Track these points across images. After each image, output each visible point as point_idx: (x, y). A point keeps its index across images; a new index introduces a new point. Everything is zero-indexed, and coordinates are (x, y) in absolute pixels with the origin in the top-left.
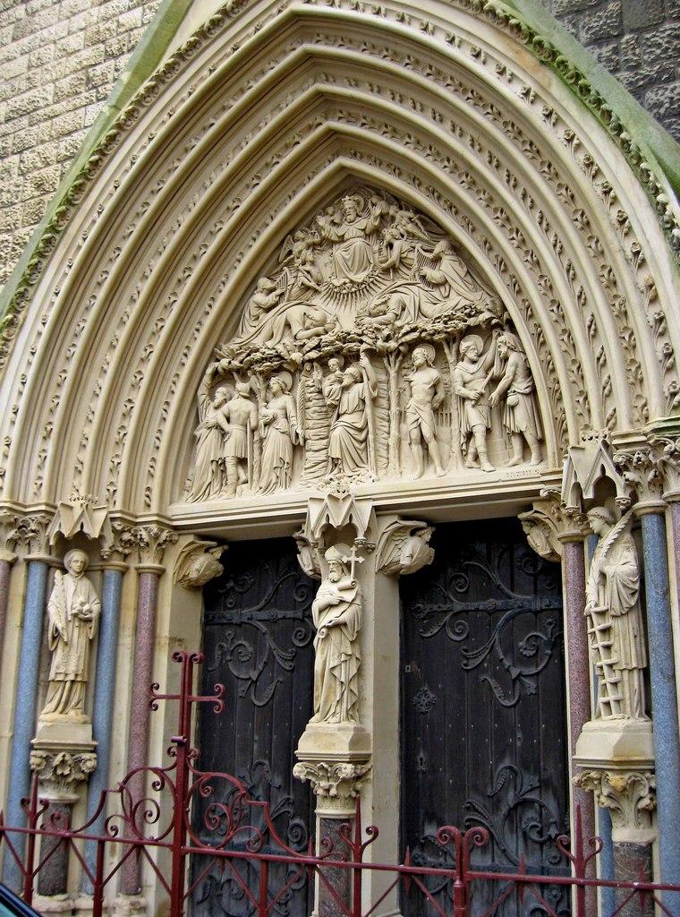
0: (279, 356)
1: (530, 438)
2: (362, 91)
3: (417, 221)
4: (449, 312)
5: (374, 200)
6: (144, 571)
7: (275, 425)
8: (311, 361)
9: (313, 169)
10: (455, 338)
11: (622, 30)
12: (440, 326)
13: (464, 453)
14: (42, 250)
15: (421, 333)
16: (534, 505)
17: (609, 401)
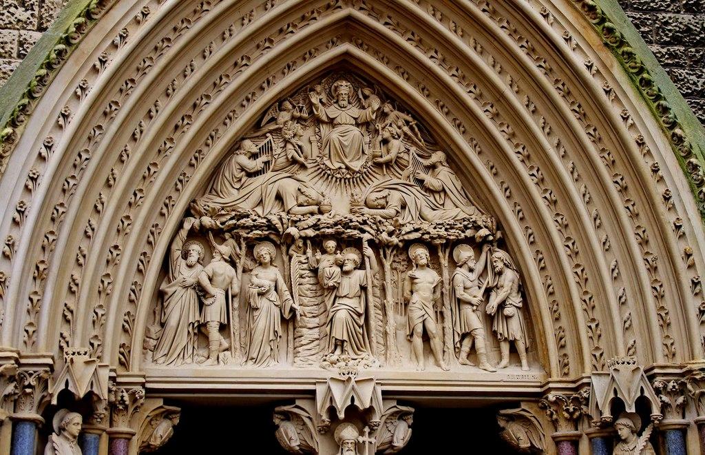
0: (270, 226)
1: (521, 347)
2: (465, 42)
3: (414, 126)
4: (452, 222)
5: (367, 92)
6: (120, 436)
7: (267, 296)
8: (305, 239)
10: (451, 245)
12: (443, 232)
13: (457, 350)
14: (54, 61)
15: (423, 234)
16: (522, 404)
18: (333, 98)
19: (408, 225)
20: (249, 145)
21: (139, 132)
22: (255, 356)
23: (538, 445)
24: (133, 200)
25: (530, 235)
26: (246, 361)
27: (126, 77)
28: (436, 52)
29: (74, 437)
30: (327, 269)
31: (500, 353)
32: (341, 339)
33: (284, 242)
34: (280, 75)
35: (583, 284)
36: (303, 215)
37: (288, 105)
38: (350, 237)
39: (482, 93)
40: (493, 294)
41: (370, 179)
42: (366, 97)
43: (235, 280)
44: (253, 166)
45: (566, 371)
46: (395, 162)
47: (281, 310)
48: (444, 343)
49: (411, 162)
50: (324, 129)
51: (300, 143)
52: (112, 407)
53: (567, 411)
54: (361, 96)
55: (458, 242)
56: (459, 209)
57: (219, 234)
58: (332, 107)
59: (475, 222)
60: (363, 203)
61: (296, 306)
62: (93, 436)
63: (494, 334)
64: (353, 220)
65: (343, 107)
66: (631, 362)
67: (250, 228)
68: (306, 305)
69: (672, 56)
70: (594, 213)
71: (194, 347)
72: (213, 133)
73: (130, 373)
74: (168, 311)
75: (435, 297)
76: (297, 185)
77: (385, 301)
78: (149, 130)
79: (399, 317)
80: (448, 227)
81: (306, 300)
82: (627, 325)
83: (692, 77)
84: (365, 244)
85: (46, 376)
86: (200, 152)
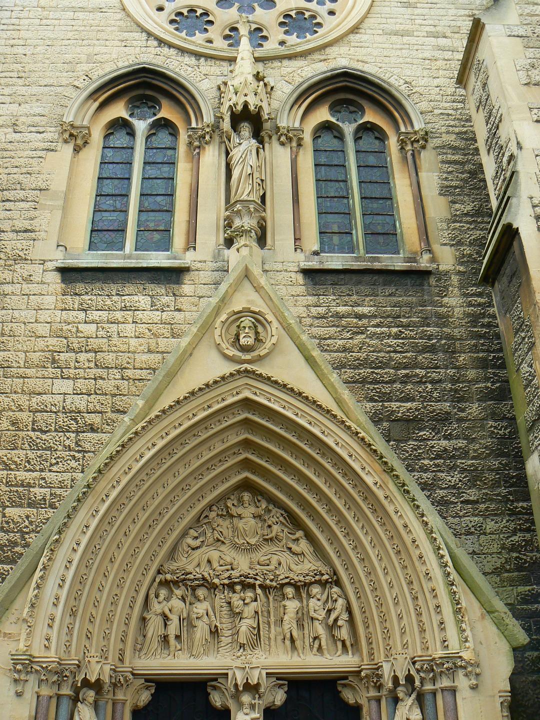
0: (204, 579)
1: (348, 644)
2: (309, 471)
4: (307, 572)
5: (259, 498)
8: (223, 585)
11: (390, 438)
12: (302, 578)
15: (290, 580)
16: (349, 677)
17: (404, 636)
20: (193, 533)
22: (194, 654)
23: (359, 701)
24: (125, 569)
27: (121, 502)
28: (295, 476)
29: (91, 704)
33: (212, 587)
35: (380, 607)
37: (214, 508)
40: (332, 612)
42: (259, 501)
43: (184, 610)
45: (372, 657)
50: (235, 520)
52: (114, 685)
53: (373, 681)
54: (256, 501)
55: (311, 583)
57: (176, 583)
59: (320, 571)
61: (218, 624)
62: (103, 702)
66: (404, 653)
67: (193, 580)
68: (224, 625)
69: (437, 466)
70: (383, 566)
73: (124, 666)
74: (147, 628)
78: (133, 530)
79: (278, 628)
82: (403, 631)
83: (448, 478)
84: (257, 587)
85: (75, 670)
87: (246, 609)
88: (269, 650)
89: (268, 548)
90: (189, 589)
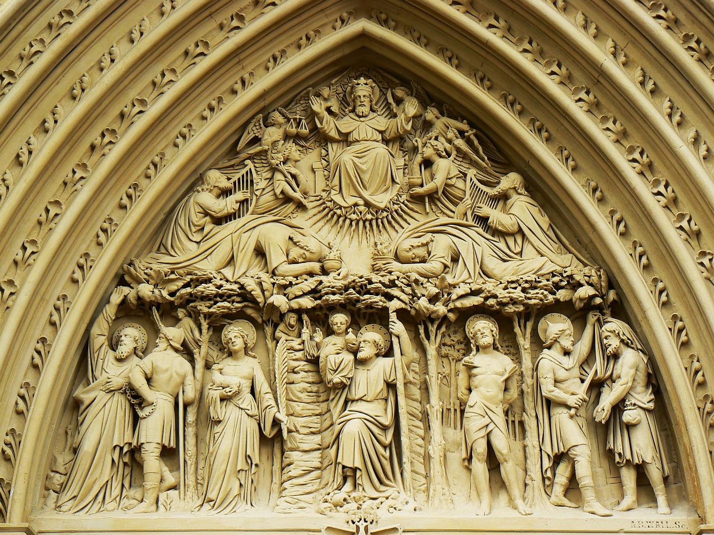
0: (245, 295)
1: (655, 474)
3: (472, 137)
4: (533, 277)
5: (400, 93)
7: (235, 400)
8: (299, 312)
9: (316, 26)
10: (535, 314)
12: (518, 294)
13: (547, 483)
15: (486, 298)
18: (349, 105)
19: (462, 285)
21: (27, 153)
25: (661, 292)
26: (202, 505)
30: (332, 358)
31: (621, 484)
32: (351, 466)
33: (267, 319)
34: (261, 70)
36: (296, 277)
38: (370, 306)
39: (570, 73)
40: (605, 390)
41: (406, 221)
42: (399, 101)
43: (189, 379)
44: (221, 207)
46: (443, 192)
47: (259, 424)
48: (526, 471)
49: (468, 192)
50: (334, 150)
51: (294, 171)
54: (391, 100)
55: (545, 310)
56: (545, 259)
57: (169, 311)
58: (347, 118)
60: (392, 255)
61: (282, 416)
63: (610, 454)
64: (374, 280)
65: (363, 117)
67: (212, 299)
68: (300, 416)
71: (123, 486)
72: (157, 159)
75: (508, 397)
76: (289, 232)
77: (428, 406)
78: (41, 150)
79: (450, 432)
80: (527, 285)
81: (298, 408)
84: (393, 317)
86: (135, 186)
87: (361, 375)
88: (428, 489)
89: (422, 219)
90: (205, 326)
